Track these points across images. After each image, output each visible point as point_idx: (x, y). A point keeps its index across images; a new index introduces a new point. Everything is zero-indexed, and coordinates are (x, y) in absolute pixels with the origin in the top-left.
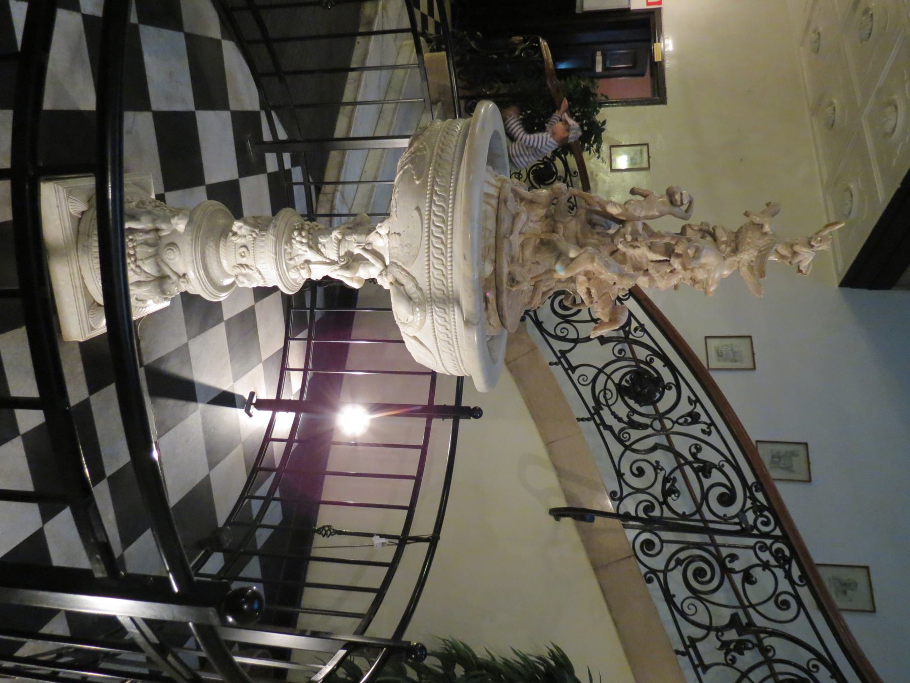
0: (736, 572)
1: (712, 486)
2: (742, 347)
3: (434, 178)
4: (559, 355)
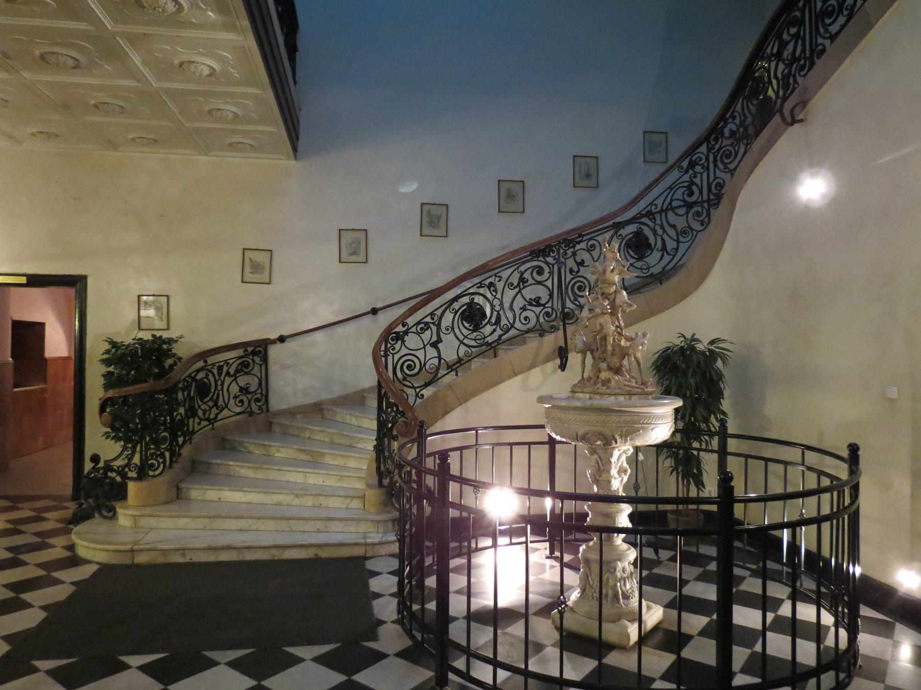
0: (247, 398)
1: (533, 279)
2: (348, 237)
3: (640, 424)
4: (450, 370)
